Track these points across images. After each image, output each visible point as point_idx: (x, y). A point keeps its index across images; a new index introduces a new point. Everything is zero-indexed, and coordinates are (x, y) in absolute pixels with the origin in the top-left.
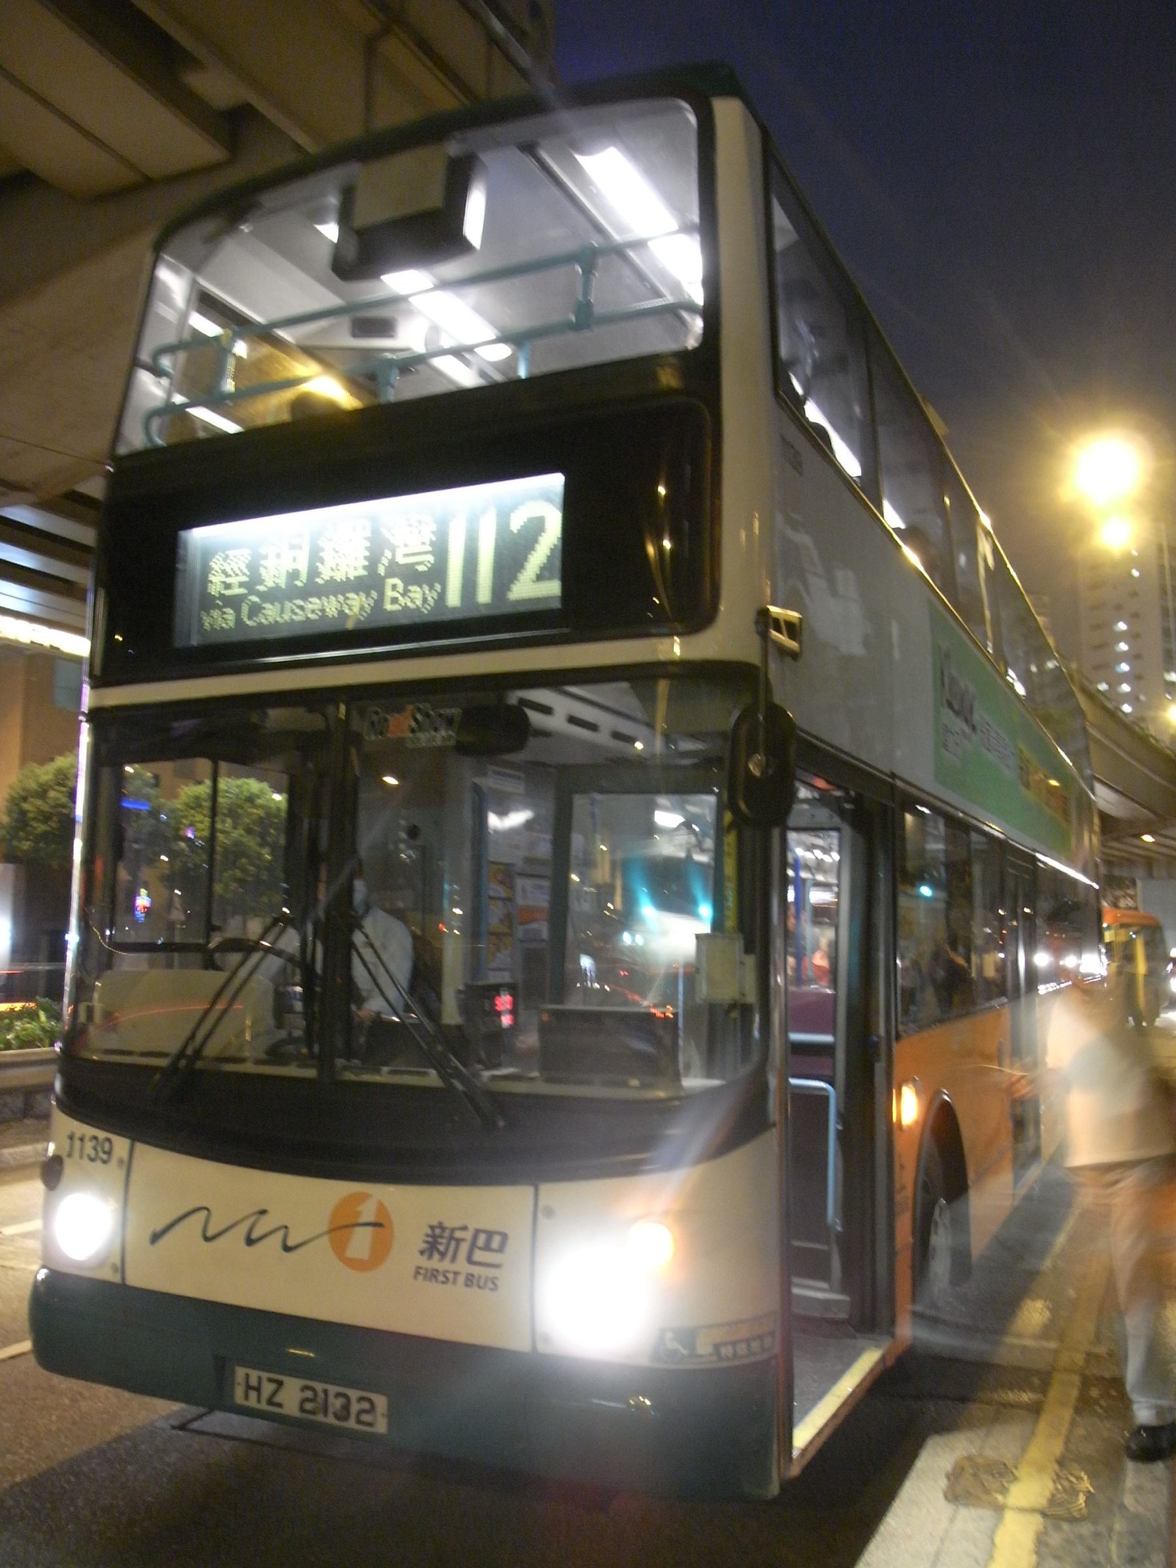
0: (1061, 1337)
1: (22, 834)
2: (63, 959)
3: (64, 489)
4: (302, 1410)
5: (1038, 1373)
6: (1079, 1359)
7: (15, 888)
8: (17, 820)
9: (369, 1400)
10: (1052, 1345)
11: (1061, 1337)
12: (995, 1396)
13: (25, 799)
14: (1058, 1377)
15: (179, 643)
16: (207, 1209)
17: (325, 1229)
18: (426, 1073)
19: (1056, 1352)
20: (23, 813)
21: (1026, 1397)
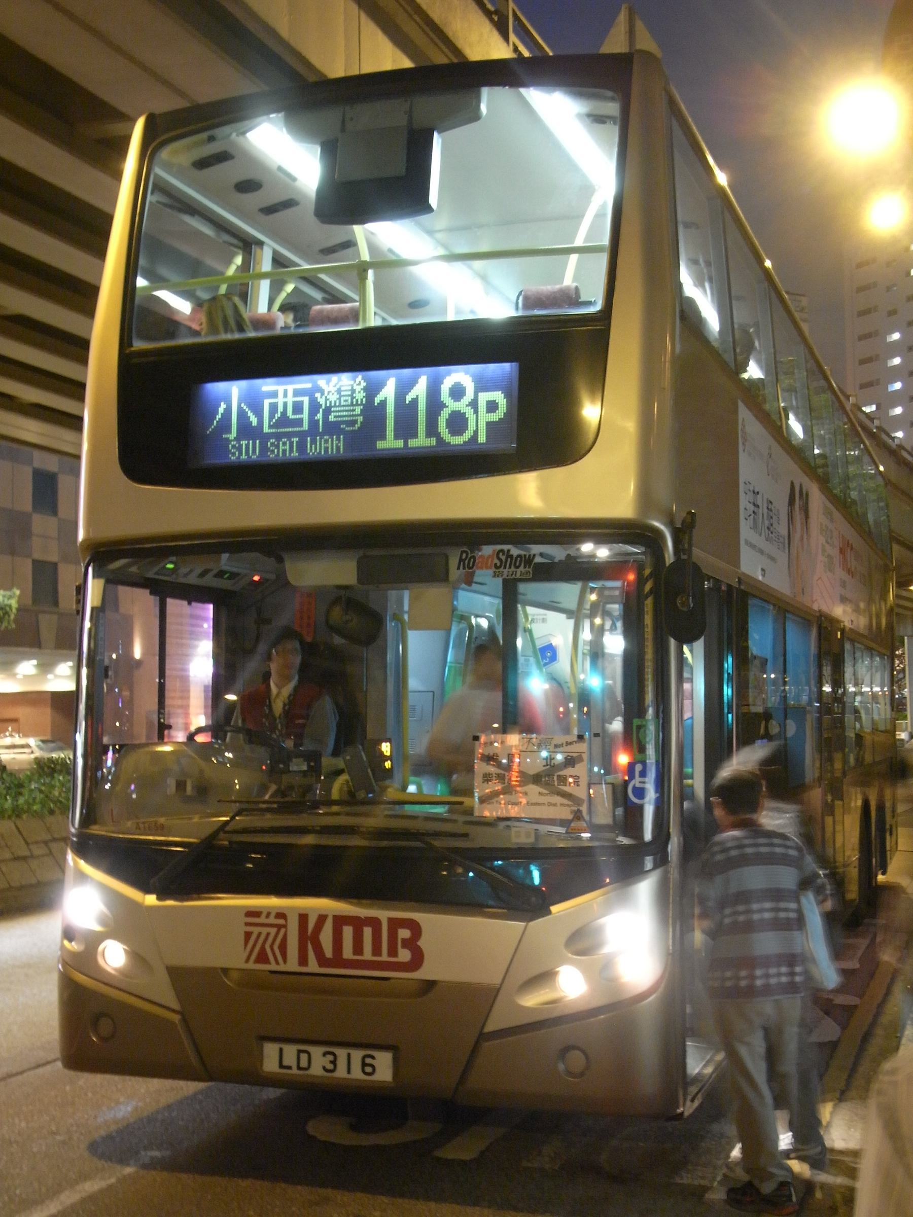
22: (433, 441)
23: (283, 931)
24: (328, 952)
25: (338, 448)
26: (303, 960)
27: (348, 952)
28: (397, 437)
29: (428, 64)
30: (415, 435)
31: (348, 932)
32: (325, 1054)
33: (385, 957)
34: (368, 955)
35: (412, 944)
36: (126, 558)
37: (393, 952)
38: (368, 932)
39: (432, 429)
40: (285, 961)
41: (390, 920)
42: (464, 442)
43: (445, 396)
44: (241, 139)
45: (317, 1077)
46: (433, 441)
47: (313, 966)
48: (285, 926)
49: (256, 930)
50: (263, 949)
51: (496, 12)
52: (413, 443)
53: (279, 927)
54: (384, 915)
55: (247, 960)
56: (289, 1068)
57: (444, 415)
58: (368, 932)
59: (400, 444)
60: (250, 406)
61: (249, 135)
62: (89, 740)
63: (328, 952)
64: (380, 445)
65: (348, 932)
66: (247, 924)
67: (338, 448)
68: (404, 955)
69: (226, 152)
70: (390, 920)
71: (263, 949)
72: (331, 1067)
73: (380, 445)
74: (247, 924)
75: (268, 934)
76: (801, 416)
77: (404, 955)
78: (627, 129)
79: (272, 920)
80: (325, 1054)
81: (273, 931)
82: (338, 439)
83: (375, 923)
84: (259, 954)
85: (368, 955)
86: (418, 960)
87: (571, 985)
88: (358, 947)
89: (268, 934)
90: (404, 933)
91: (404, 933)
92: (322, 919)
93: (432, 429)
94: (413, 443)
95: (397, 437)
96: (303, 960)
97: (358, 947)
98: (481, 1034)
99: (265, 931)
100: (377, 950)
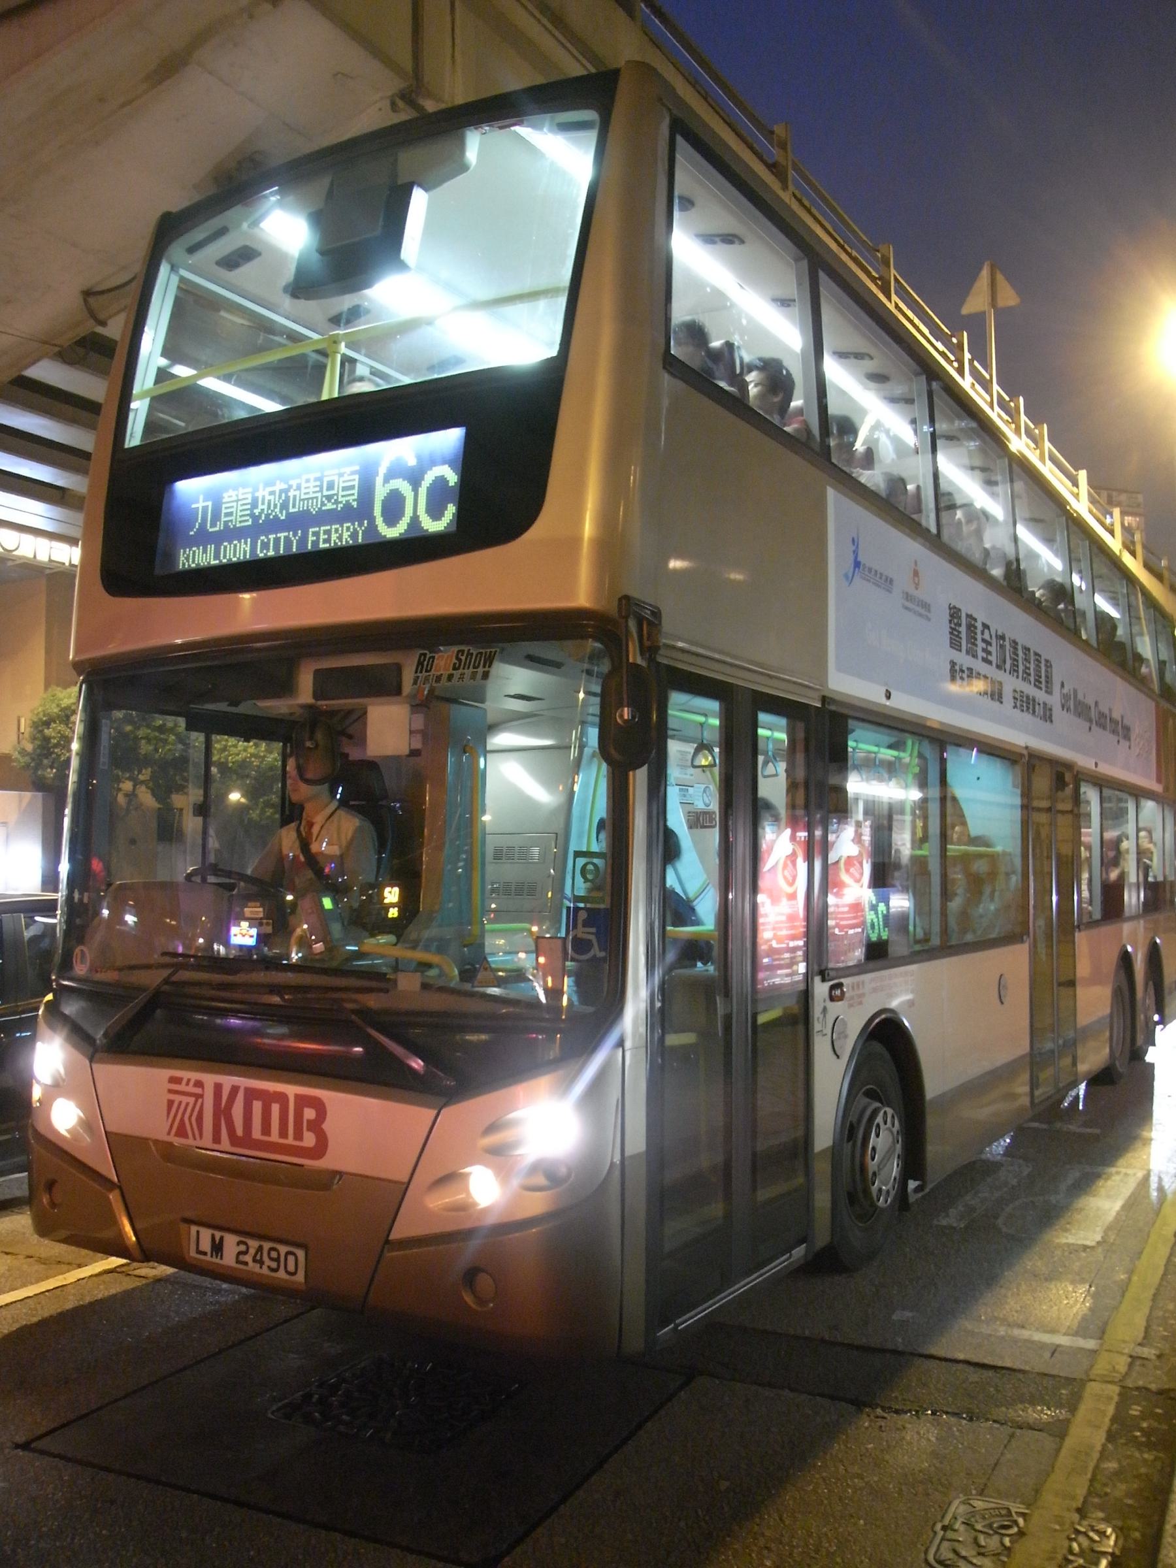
0: (1101, 1334)
1: (45, 761)
2: (397, 370)
3: (14, 374)
4: (238, 1262)
5: (1070, 1381)
6: (1122, 1363)
7: (44, 833)
8: (41, 747)
9: (246, 1244)
10: (1091, 1344)
11: (1101, 1334)
12: (1011, 1413)
13: (47, 724)
14: (1092, 1388)
15: (158, 571)
16: (248, 1249)
17: (87, 1062)
18: (874, 1149)
19: (1094, 1352)
20: (47, 739)
21: (1045, 1414)
23: (200, 1101)
24: (240, 1132)
25: (245, 552)
26: (217, 1139)
27: (257, 1134)
31: (257, 1106)
32: (239, 1243)
33: (290, 1141)
34: (275, 1137)
35: (316, 1126)
36: (981, 269)
37: (299, 1136)
38: (275, 1108)
40: (201, 1137)
41: (297, 1096)
44: (256, 230)
45: (229, 1267)
47: (225, 1144)
48: (201, 1096)
49: (177, 1098)
50: (182, 1120)
51: (879, 279)
53: (198, 1097)
54: (291, 1090)
55: (169, 1134)
56: (205, 1254)
58: (275, 1108)
60: (225, 503)
61: (262, 225)
63: (240, 1132)
65: (257, 1106)
66: (170, 1091)
67: (245, 552)
68: (309, 1140)
69: (246, 247)
74: (170, 1091)
75: (187, 1104)
77: (309, 1140)
79: (191, 1089)
80: (239, 1243)
81: (192, 1100)
82: (246, 543)
83: (282, 1098)
84: (178, 1128)
86: (321, 1149)
87: (485, 1190)
88: (266, 1130)
89: (187, 1104)
90: (309, 1114)
91: (309, 1114)
92: (235, 1090)
96: (217, 1139)
98: (387, 1242)
99: (185, 1099)
100: (283, 1133)
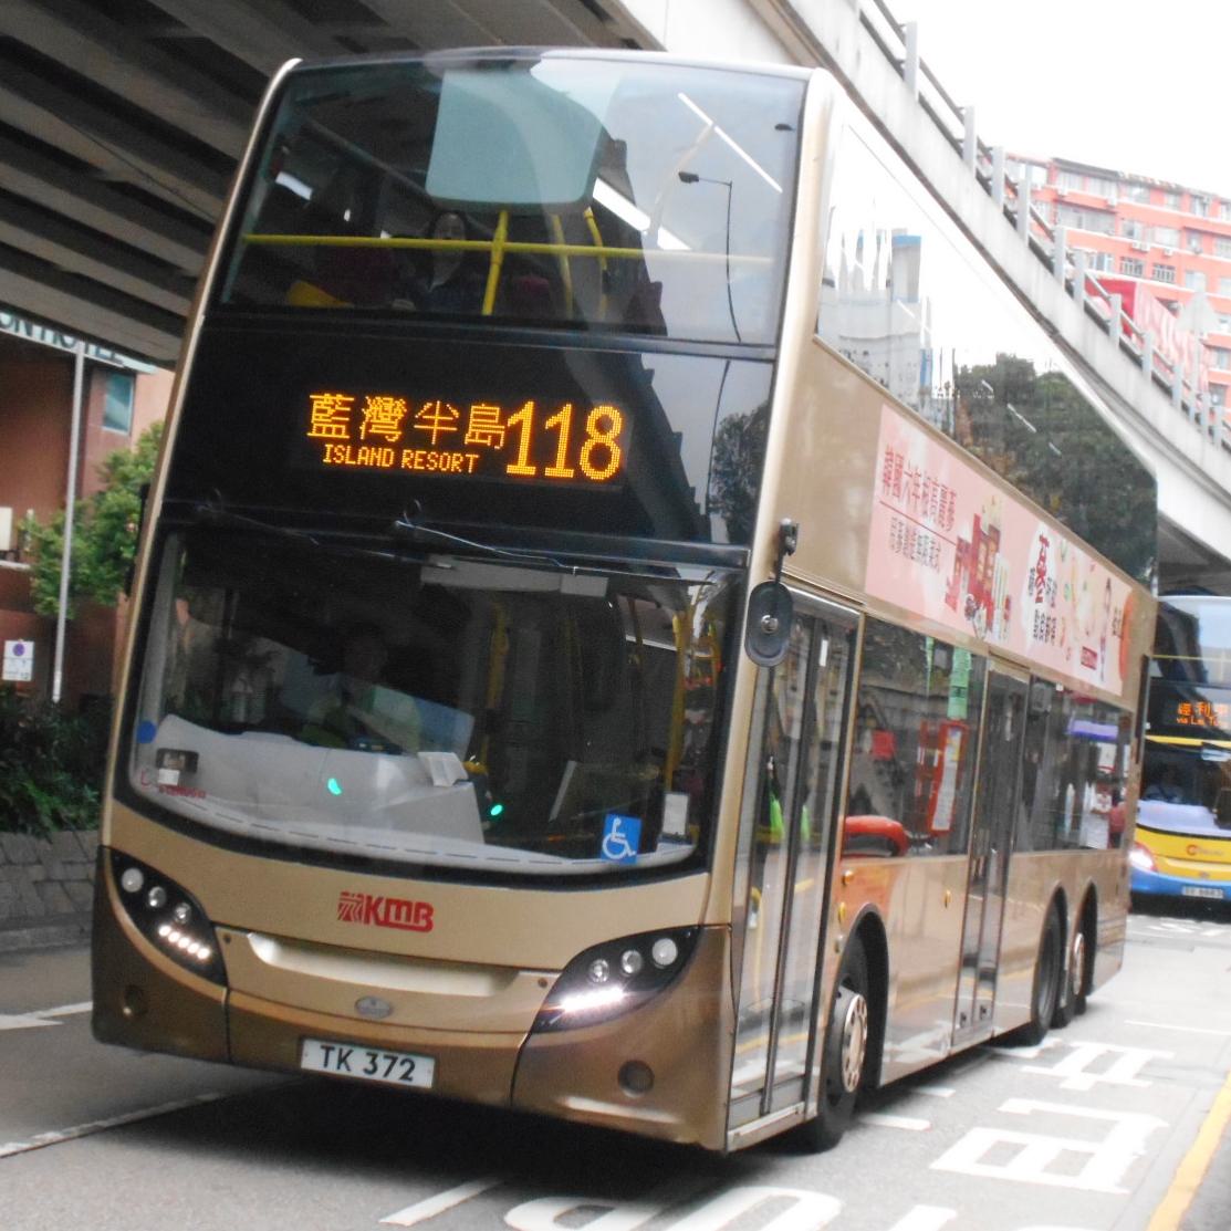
22: (570, 473)
27: (392, 918)
28: (530, 463)
29: (424, 703)
30: (553, 465)
31: (393, 909)
33: (412, 923)
34: (403, 921)
37: (417, 920)
38: (404, 909)
39: (573, 460)
42: (606, 478)
43: (591, 428)
46: (570, 473)
50: (348, 912)
52: (549, 472)
53: (358, 903)
57: (587, 447)
58: (404, 909)
59: (531, 471)
62: (1058, 948)
63: (381, 915)
64: (511, 469)
65: (393, 909)
68: (423, 923)
70: (91, 366)
71: (348, 912)
72: (370, 1067)
73: (511, 469)
76: (1070, 393)
78: (317, 943)
79: (355, 898)
85: (403, 921)
88: (398, 916)
93: (573, 460)
94: (549, 472)
95: (530, 463)
97: (398, 916)
99: (350, 903)
100: (408, 918)
